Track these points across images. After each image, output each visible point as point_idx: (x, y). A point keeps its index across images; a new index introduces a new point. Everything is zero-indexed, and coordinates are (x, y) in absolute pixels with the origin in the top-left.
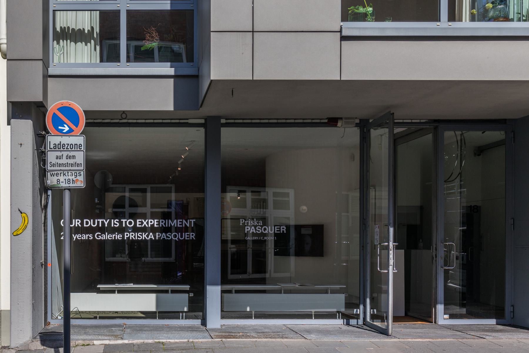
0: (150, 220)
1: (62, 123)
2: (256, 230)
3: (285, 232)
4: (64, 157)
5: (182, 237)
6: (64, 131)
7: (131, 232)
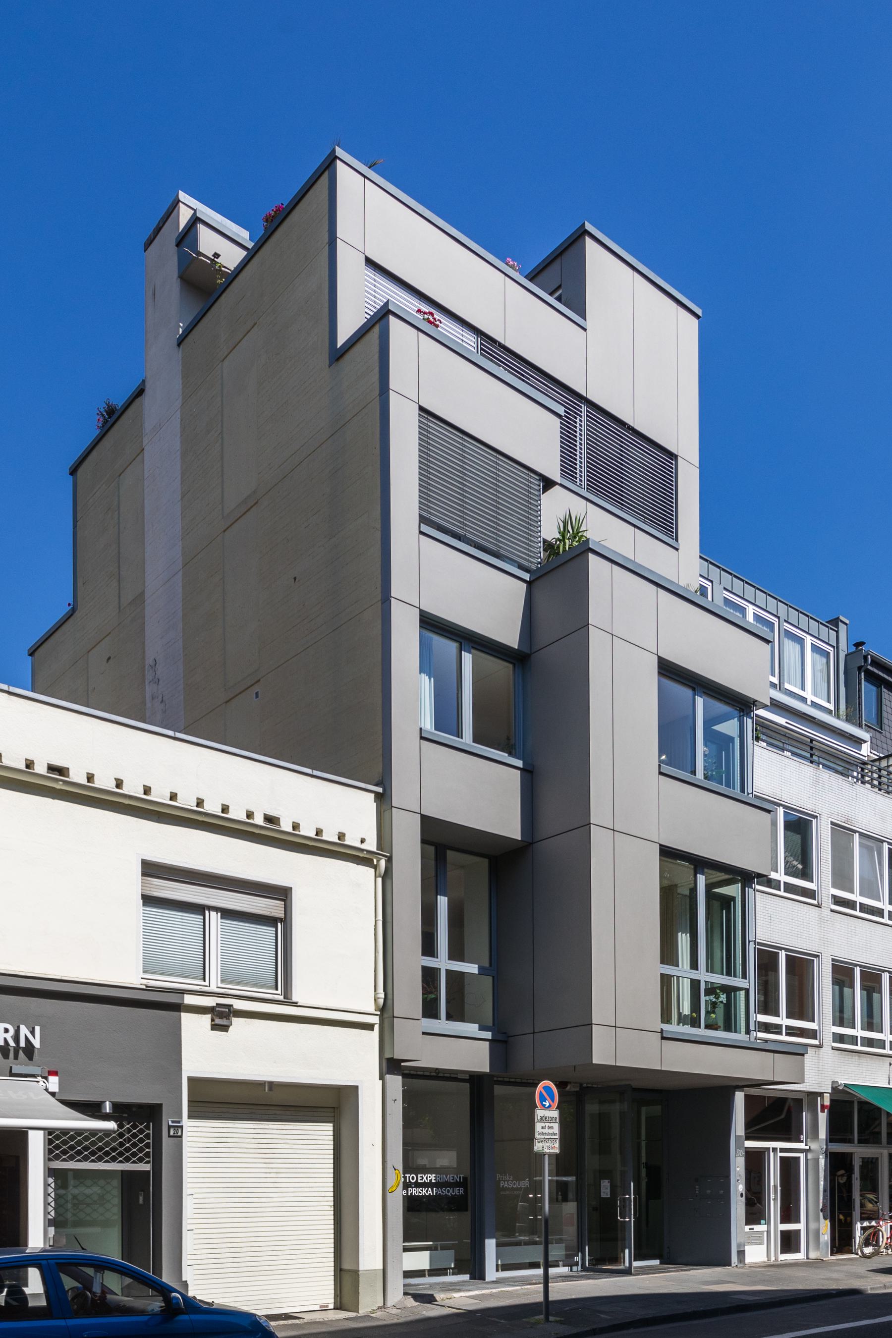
0: (429, 1175)
1: (545, 1100)
2: (508, 1185)
3: (528, 1186)
4: (547, 1128)
5: (453, 1192)
6: (546, 1106)
7: (414, 1187)
